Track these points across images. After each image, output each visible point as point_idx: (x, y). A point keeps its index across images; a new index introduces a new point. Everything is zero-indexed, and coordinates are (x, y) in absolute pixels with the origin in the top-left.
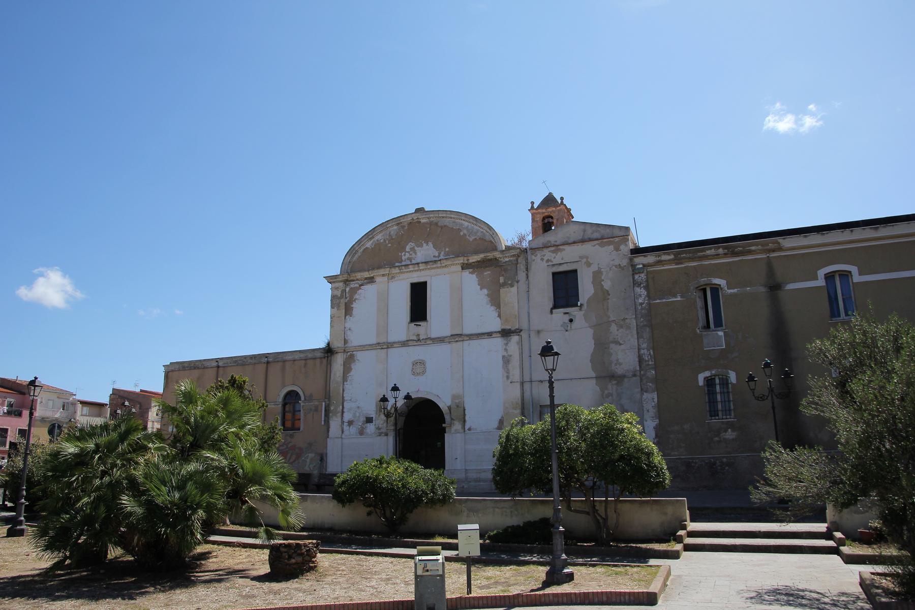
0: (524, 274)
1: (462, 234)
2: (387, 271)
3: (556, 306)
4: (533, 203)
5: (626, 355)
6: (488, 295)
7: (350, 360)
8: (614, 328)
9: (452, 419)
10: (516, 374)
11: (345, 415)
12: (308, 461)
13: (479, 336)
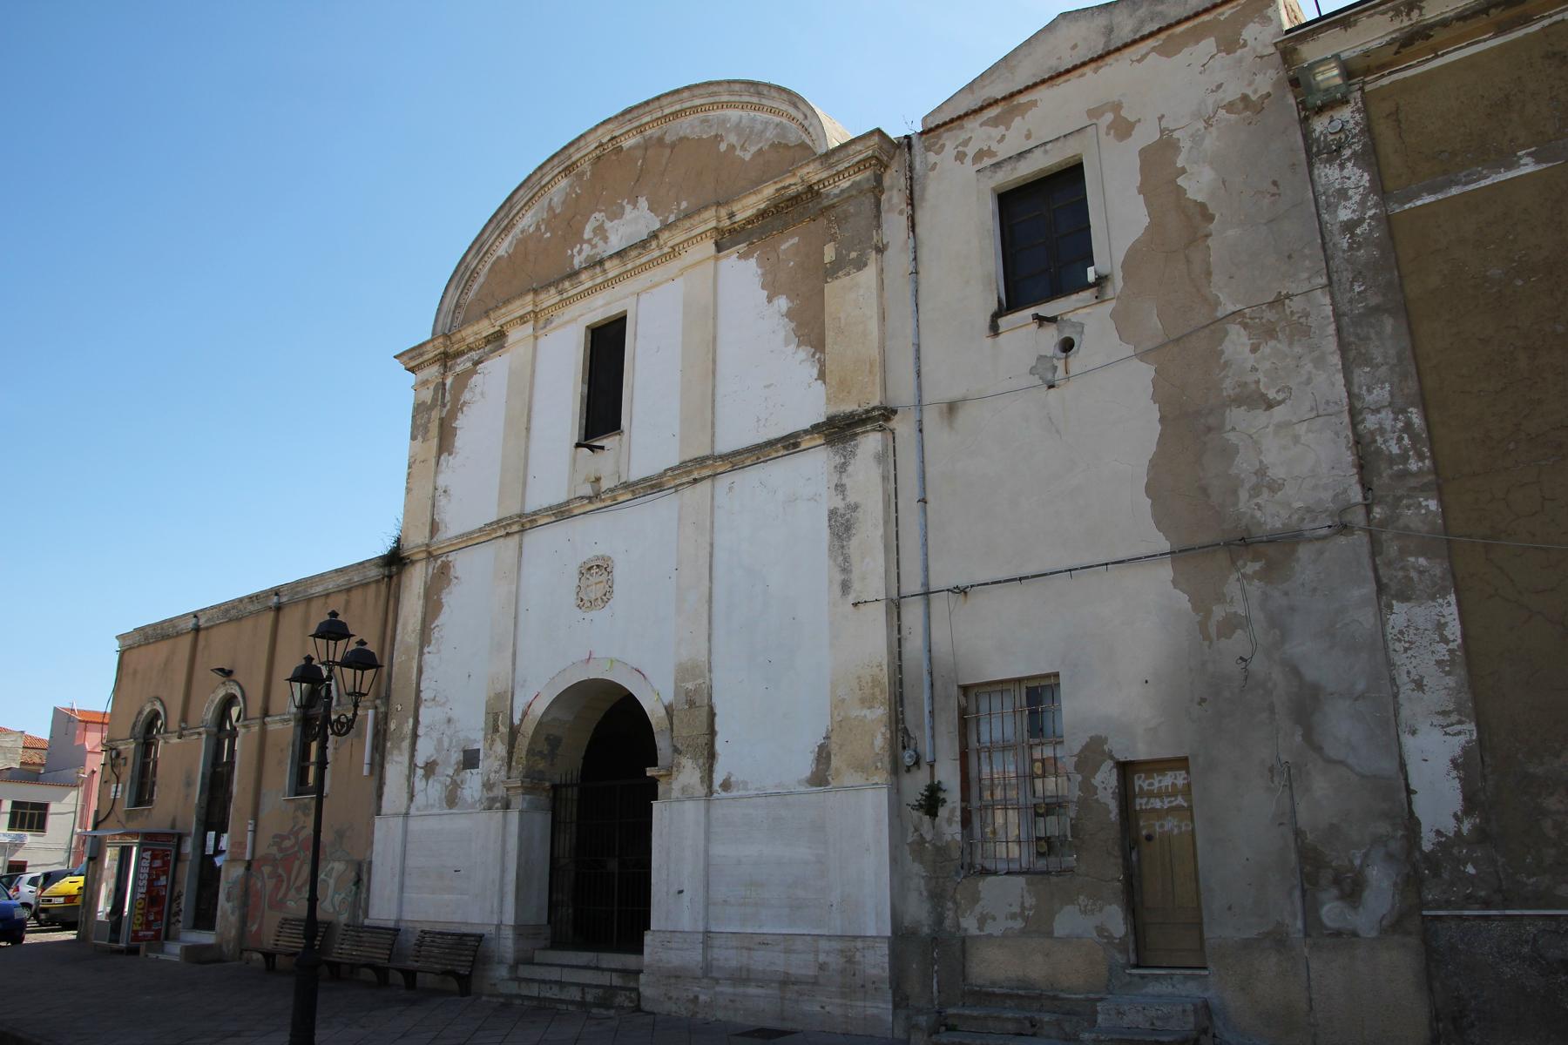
0: (903, 221)
1: (723, 147)
2: (524, 305)
3: (1013, 301)
5: (1296, 454)
6: (790, 315)
7: (441, 578)
8: (1237, 343)
9: (676, 750)
10: (872, 578)
11: (420, 744)
12: (332, 882)
13: (760, 452)
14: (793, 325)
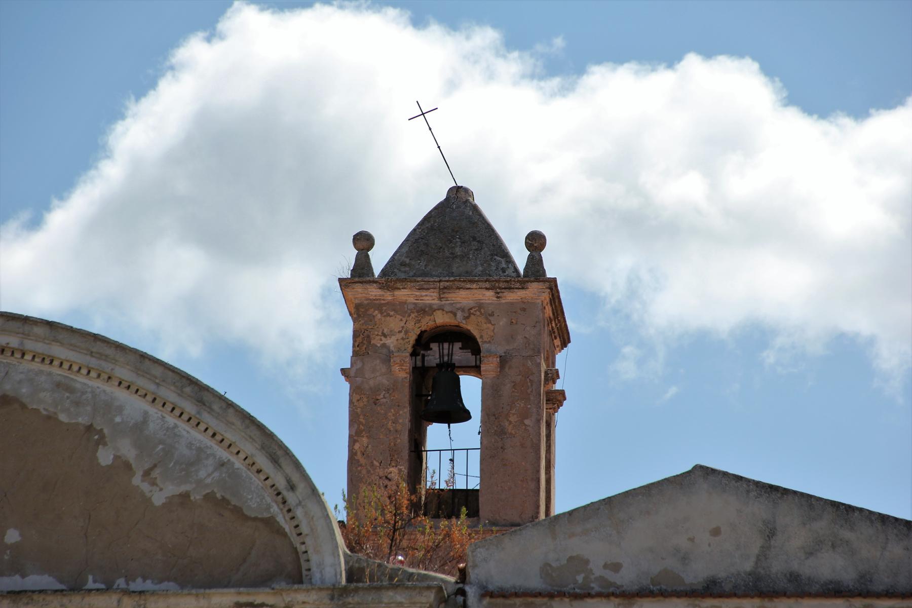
1: (105, 457)
4: (364, 241)
14: (55, 202)
